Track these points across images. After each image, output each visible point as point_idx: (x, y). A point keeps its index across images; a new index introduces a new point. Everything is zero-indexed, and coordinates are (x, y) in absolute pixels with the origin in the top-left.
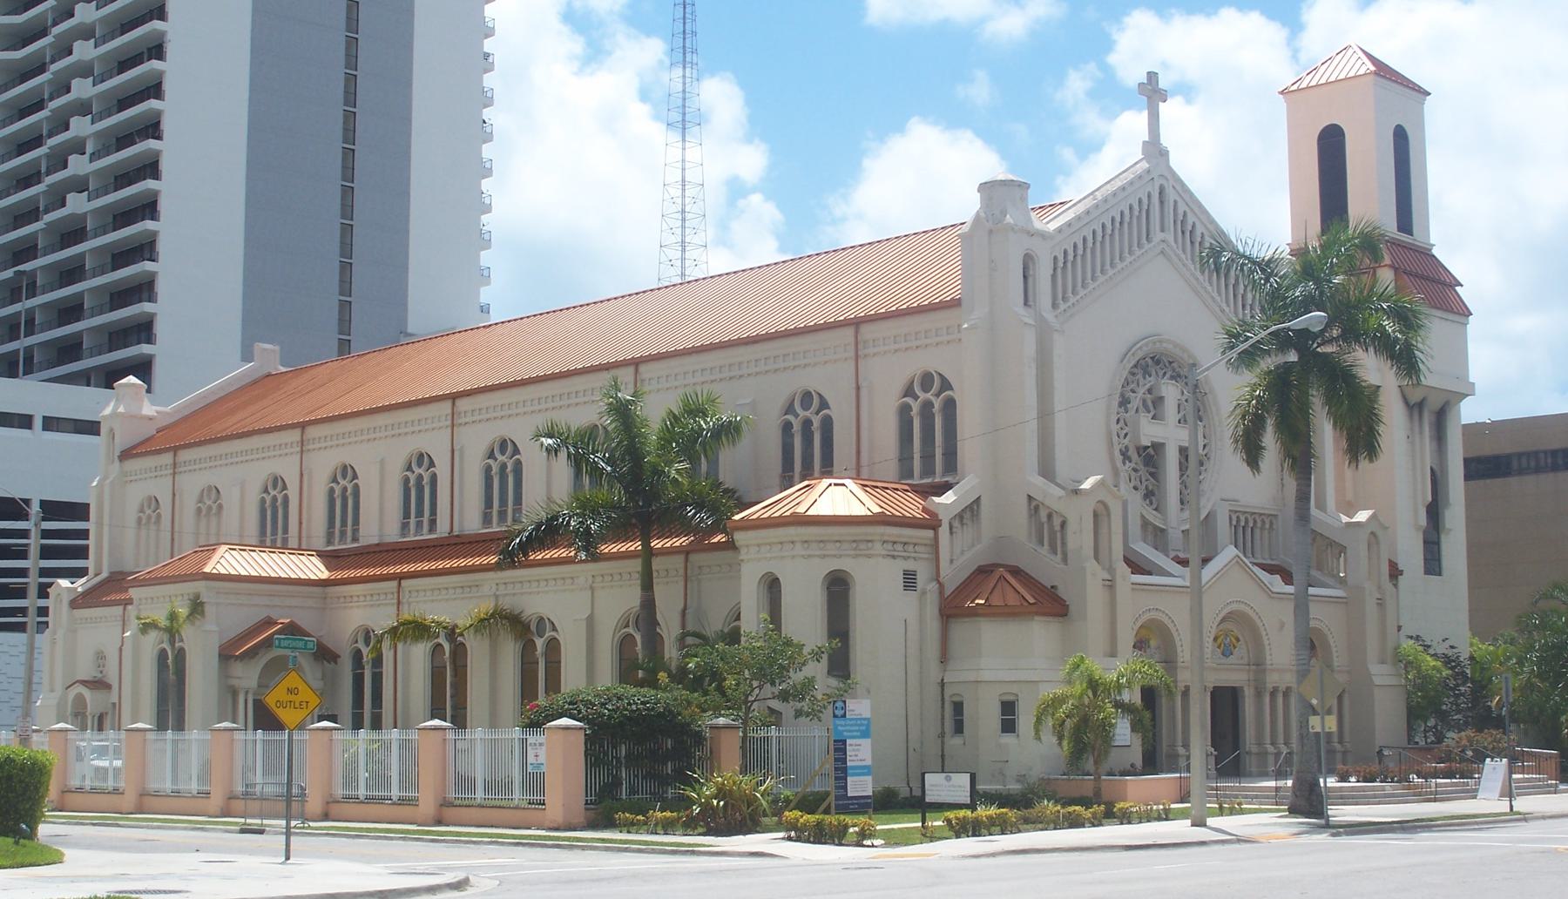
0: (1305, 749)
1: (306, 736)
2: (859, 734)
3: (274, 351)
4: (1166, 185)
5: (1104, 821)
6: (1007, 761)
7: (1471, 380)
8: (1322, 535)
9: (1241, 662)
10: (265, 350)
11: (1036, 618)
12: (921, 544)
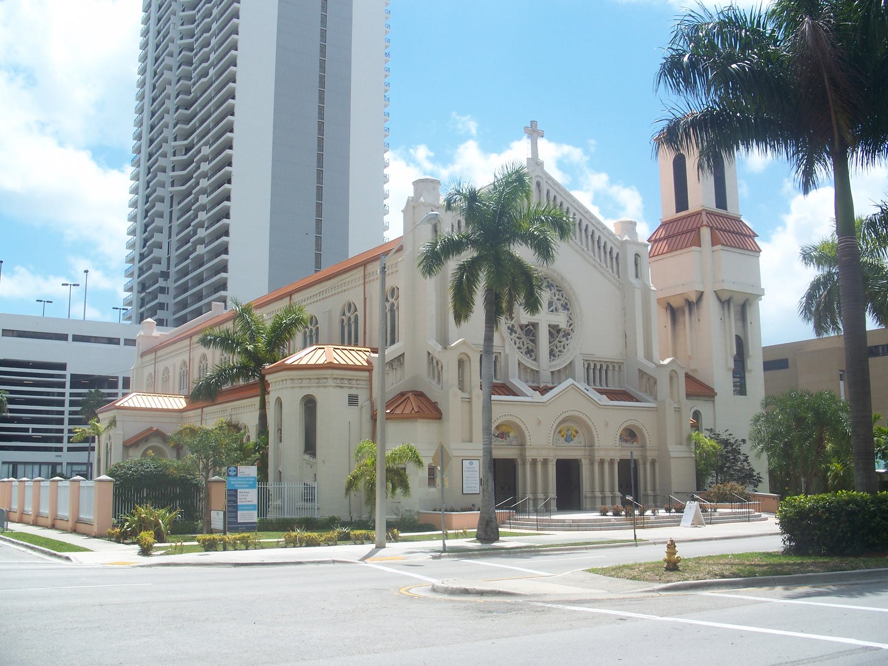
0: (485, 498)
1: (67, 483)
2: (247, 486)
3: (221, 305)
4: (541, 181)
5: (338, 542)
6: (400, 502)
7: (762, 287)
8: (646, 373)
9: (580, 445)
10: (216, 305)
11: (419, 420)
12: (362, 380)
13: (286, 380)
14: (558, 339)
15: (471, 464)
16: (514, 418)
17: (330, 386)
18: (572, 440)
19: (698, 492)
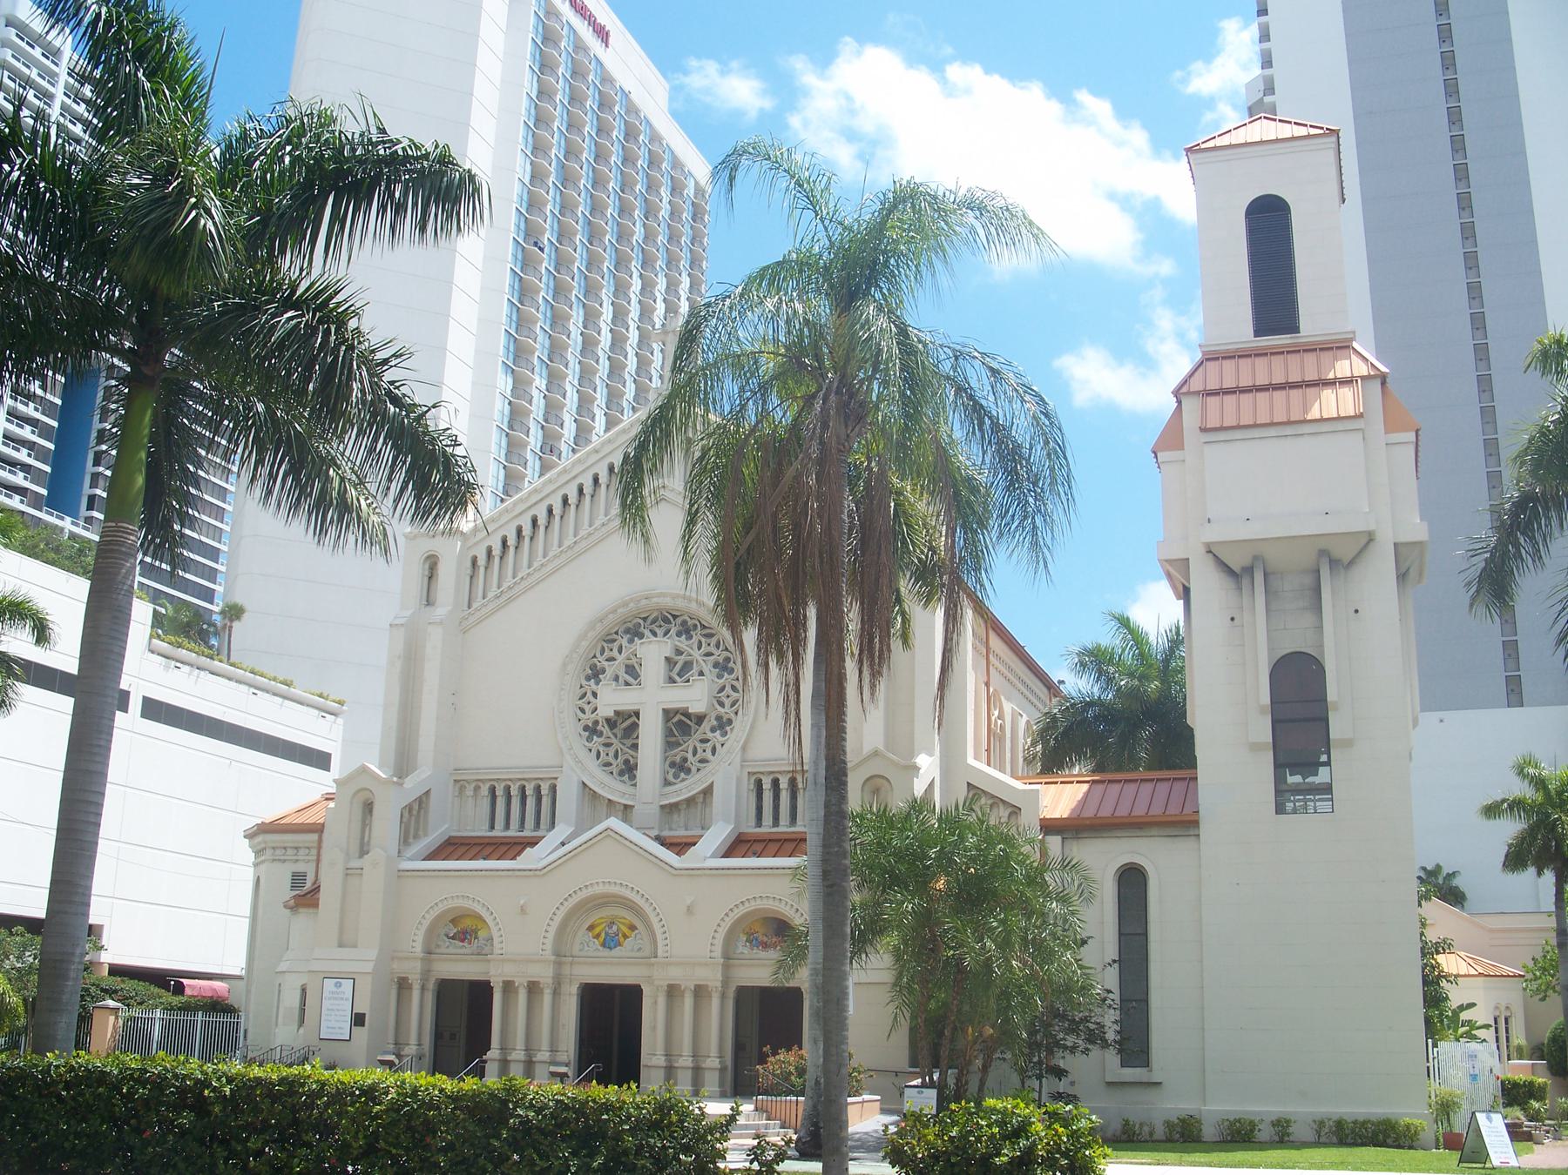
9: (638, 954)
14: (698, 736)
15: (338, 985)
18: (620, 945)
19: (911, 1070)
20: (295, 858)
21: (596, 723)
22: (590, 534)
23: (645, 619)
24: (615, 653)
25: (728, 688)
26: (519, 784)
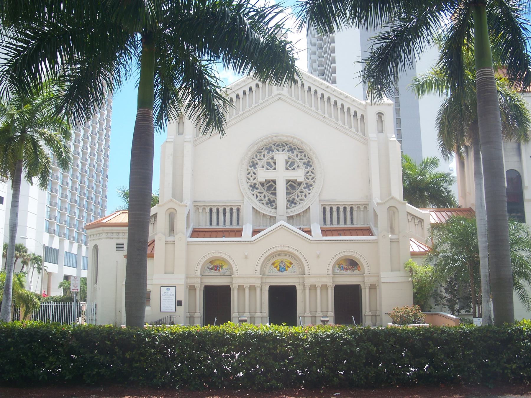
13: (102, 233)
14: (299, 190)
16: (222, 254)
17: (103, 238)
20: (118, 237)
21: (255, 184)
22: (250, 110)
23: (274, 144)
24: (262, 157)
25: (310, 172)
26: (223, 207)
